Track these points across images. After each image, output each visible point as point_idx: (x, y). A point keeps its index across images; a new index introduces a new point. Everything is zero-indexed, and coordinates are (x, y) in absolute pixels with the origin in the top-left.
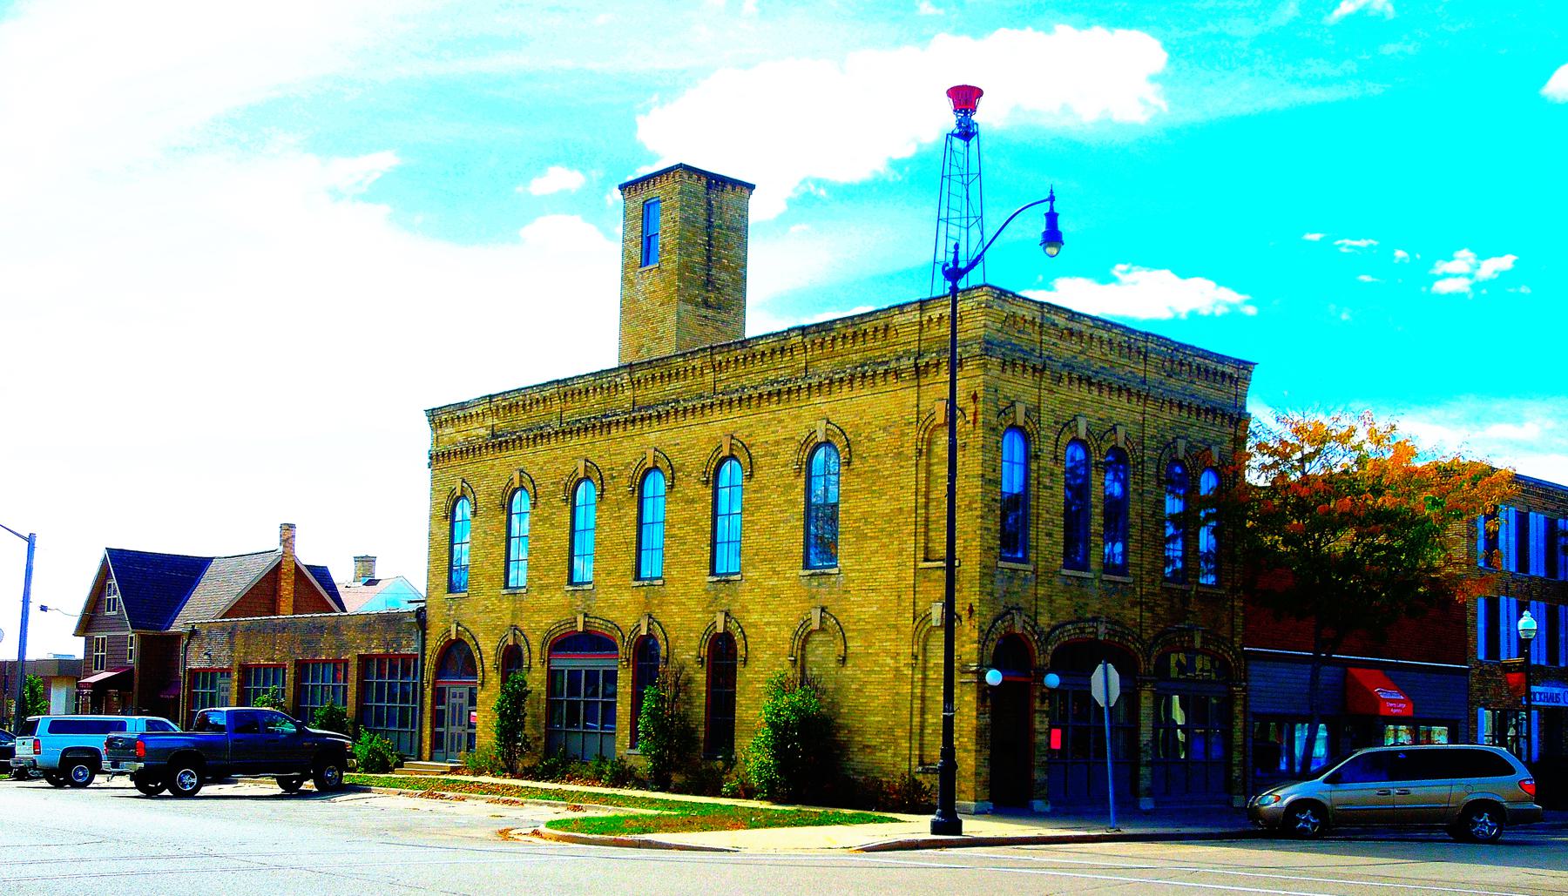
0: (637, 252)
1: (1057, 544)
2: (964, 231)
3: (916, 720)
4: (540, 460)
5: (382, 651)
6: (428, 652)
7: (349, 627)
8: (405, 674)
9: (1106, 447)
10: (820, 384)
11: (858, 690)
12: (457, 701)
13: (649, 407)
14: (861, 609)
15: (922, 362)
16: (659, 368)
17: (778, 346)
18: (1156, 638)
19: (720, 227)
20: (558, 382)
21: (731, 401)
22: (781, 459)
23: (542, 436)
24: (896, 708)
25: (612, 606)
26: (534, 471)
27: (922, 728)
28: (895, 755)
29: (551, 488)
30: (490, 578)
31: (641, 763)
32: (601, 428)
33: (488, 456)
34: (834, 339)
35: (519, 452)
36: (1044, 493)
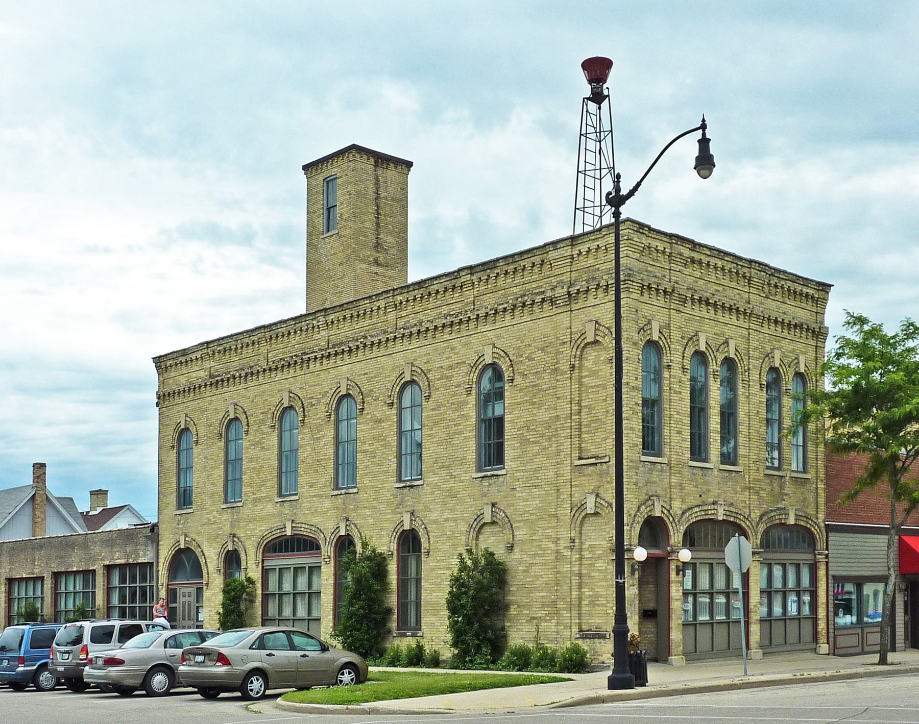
0: (320, 222)
1: (684, 440)
2: (598, 181)
3: (575, 593)
4: (251, 394)
5: (123, 561)
6: (161, 560)
7: (95, 542)
8: (144, 579)
9: (720, 357)
10: (487, 314)
11: (524, 571)
12: (187, 599)
13: (341, 344)
14: (524, 503)
15: (573, 290)
16: (350, 309)
17: (449, 285)
18: (761, 517)
19: (386, 198)
20: (264, 327)
21: (411, 334)
22: (455, 381)
23: (252, 374)
24: (557, 584)
25: (315, 513)
26: (245, 404)
27: (580, 599)
28: (558, 624)
29: (261, 417)
30: (213, 495)
31: (447, 653)
32: (302, 363)
33: (207, 392)
34: (498, 275)
35: (232, 388)
36: (675, 397)
